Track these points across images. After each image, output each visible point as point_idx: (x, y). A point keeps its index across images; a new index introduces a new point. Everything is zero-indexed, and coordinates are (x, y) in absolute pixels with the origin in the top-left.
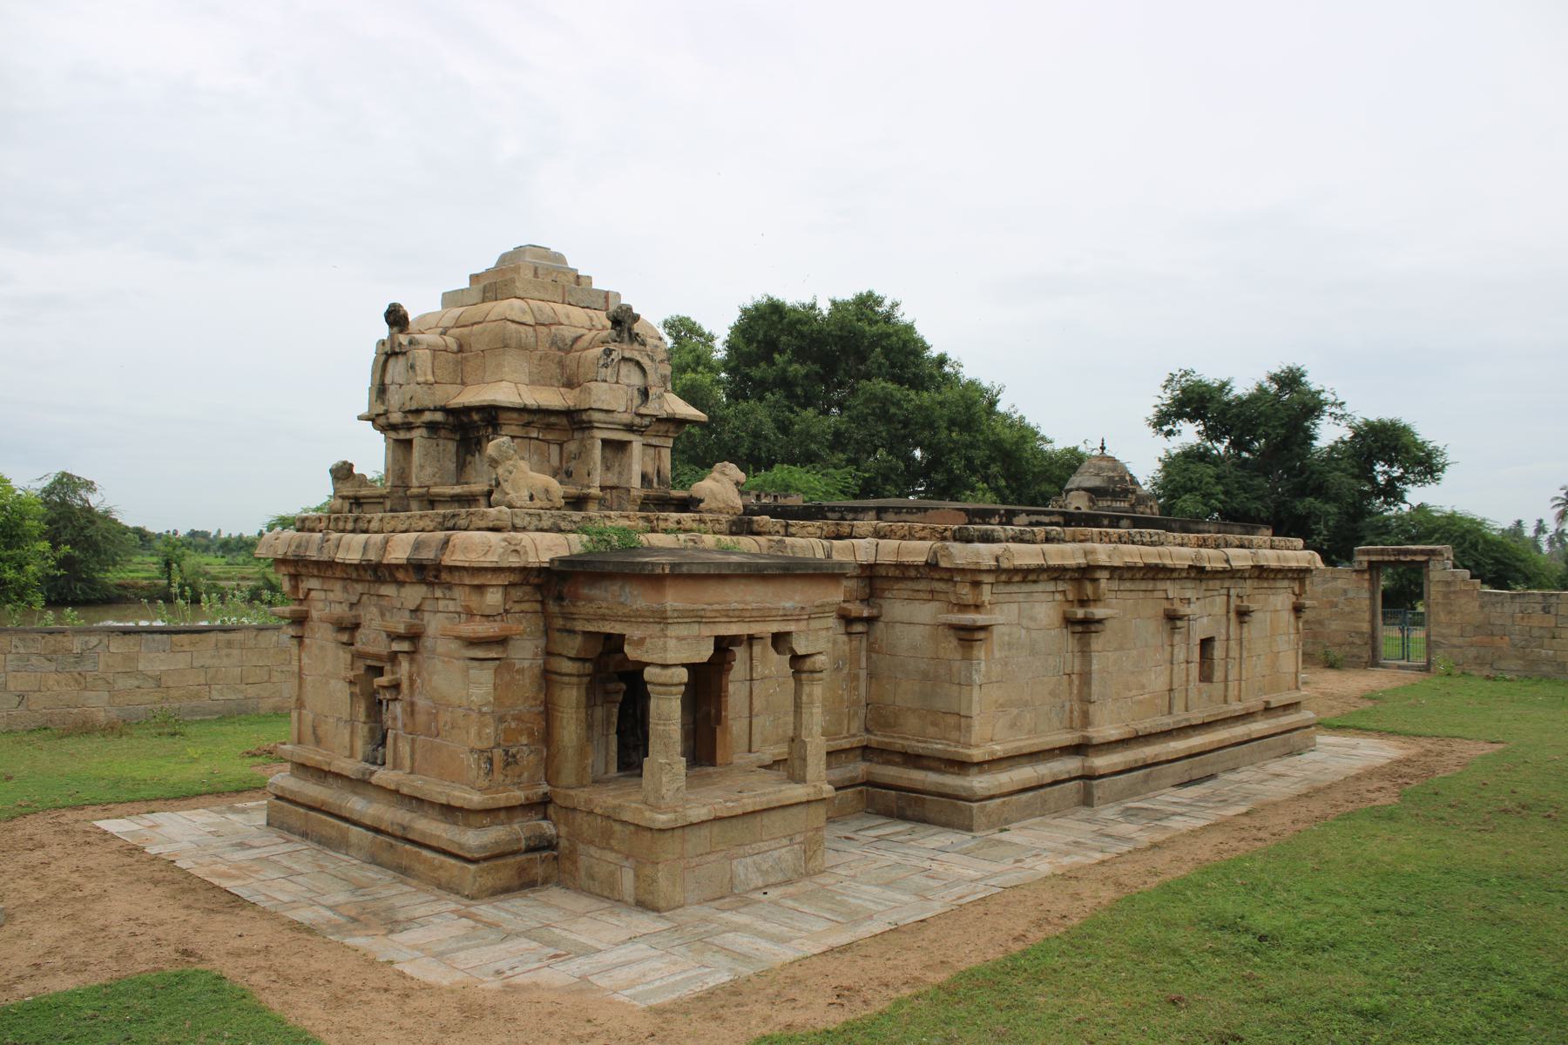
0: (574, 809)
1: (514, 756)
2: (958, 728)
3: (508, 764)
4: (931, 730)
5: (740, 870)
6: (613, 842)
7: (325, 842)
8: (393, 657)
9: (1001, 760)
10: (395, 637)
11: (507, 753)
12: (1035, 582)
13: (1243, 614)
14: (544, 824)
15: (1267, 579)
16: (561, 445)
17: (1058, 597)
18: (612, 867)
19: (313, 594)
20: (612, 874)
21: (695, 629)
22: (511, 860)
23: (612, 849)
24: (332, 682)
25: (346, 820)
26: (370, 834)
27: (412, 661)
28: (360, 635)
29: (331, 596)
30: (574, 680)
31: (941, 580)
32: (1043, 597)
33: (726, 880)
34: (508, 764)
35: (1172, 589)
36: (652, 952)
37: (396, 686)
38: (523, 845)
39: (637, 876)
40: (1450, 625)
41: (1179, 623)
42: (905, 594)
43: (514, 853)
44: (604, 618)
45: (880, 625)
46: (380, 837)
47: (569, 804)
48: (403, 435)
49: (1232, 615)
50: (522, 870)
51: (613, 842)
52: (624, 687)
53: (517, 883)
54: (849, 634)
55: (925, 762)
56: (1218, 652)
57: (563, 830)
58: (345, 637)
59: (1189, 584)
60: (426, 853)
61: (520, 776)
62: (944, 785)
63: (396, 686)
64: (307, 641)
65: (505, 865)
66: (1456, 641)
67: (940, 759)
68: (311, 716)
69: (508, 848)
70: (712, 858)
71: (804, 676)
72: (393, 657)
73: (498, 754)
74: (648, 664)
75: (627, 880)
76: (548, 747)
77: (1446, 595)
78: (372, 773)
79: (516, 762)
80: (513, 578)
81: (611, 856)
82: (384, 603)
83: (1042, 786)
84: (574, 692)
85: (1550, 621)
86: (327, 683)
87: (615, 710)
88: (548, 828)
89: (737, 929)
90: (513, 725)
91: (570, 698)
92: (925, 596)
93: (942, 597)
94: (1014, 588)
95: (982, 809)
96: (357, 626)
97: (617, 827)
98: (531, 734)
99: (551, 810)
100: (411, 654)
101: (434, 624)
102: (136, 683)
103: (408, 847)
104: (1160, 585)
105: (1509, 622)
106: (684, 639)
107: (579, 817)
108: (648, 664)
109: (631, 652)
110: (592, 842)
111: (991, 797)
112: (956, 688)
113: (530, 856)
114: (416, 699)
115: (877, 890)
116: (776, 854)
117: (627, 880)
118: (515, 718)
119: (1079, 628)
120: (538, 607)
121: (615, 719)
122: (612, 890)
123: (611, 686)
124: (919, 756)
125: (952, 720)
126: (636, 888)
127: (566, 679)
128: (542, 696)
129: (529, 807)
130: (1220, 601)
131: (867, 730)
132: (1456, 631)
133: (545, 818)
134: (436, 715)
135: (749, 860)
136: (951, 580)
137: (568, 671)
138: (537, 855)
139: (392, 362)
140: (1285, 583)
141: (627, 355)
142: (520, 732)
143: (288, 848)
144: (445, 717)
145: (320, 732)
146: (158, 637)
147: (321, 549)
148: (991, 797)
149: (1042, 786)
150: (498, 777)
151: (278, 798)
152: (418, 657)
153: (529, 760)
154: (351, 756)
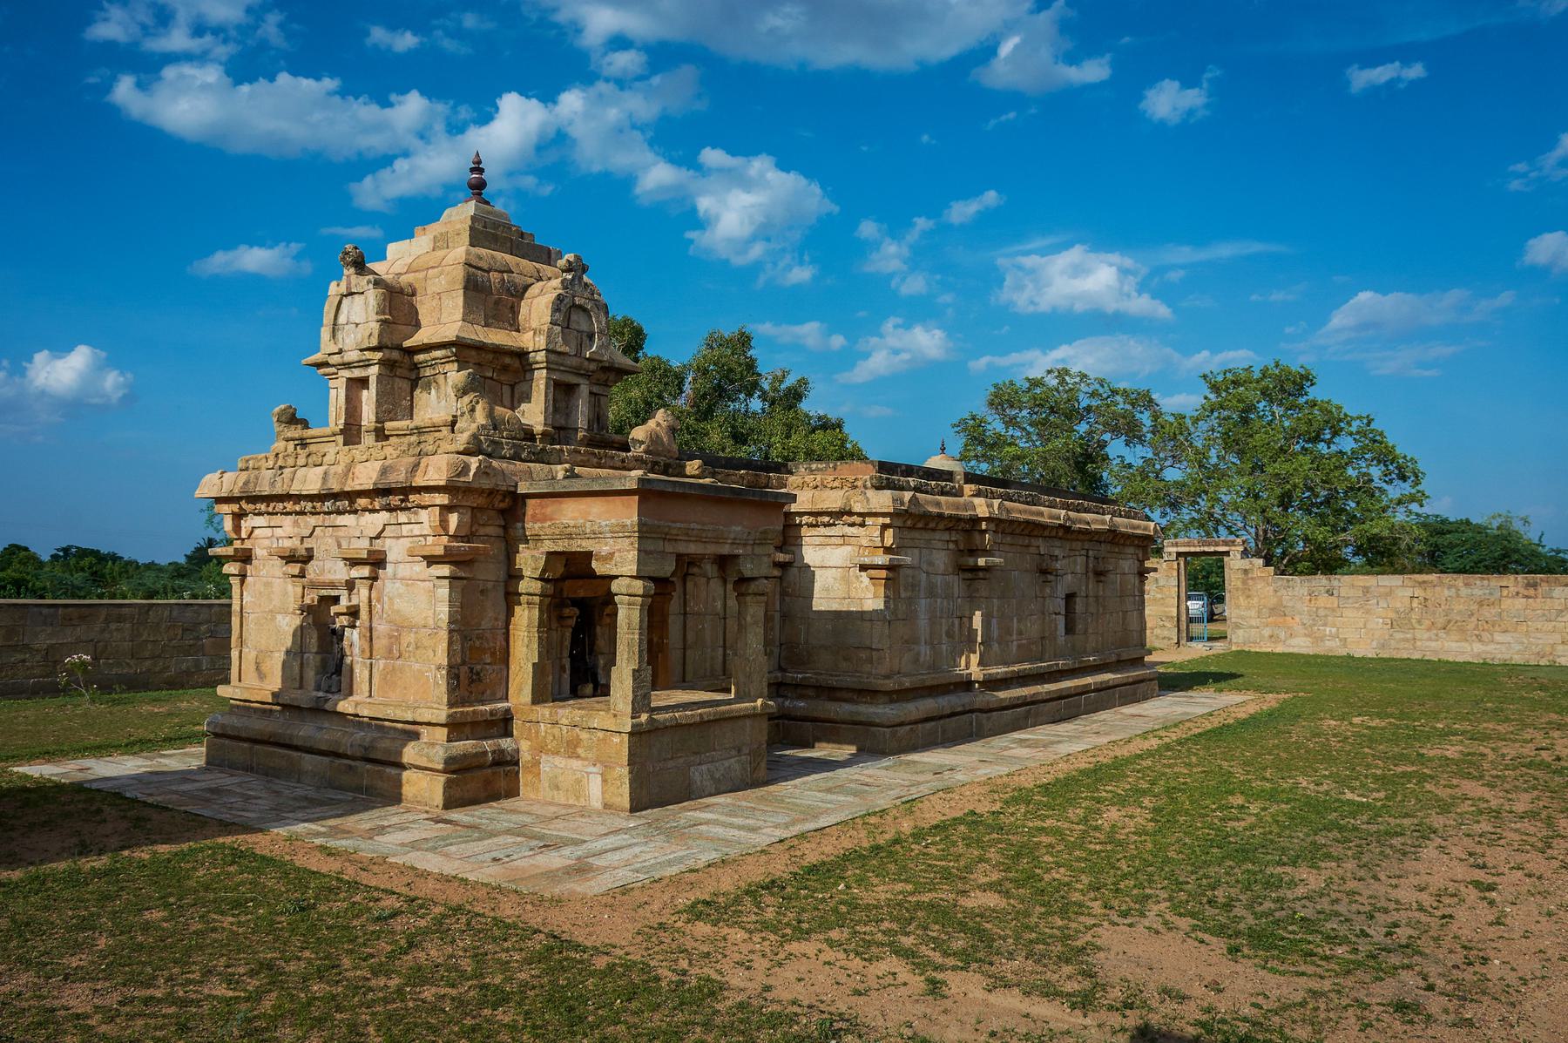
4: (844, 665)
5: (697, 777)
6: (580, 751)
7: (270, 773)
8: (350, 585)
9: (907, 690)
10: (354, 562)
12: (933, 530)
13: (1100, 574)
15: (1117, 544)
16: (512, 387)
17: (952, 546)
18: (579, 775)
19: (257, 532)
20: (578, 781)
21: (660, 545)
24: (279, 617)
25: (297, 748)
26: (326, 760)
28: (312, 568)
29: (278, 532)
32: (940, 545)
35: (1043, 546)
36: (1142, 304)
37: (354, 613)
39: (604, 781)
40: (1248, 608)
41: (1050, 578)
42: (818, 540)
45: (794, 571)
46: (338, 761)
48: (357, 373)
49: (1091, 575)
51: (580, 751)
52: (577, 611)
55: (838, 694)
56: (1079, 606)
58: (295, 569)
59: (1058, 543)
64: (249, 579)
66: (1254, 623)
67: (853, 690)
68: (253, 654)
71: (748, 598)
72: (350, 585)
74: (616, 577)
77: (1244, 582)
78: (327, 700)
80: (481, 501)
81: (576, 764)
82: (341, 533)
83: (941, 717)
86: (273, 619)
87: (568, 634)
89: (707, 822)
92: (840, 541)
94: (916, 534)
96: (308, 557)
97: (584, 735)
101: (395, 550)
103: (369, 766)
104: (1035, 542)
106: (651, 553)
109: (598, 567)
111: (902, 724)
112: (868, 624)
115: (820, 795)
116: (726, 764)
119: (969, 575)
120: (500, 531)
121: (567, 643)
123: (567, 611)
124: (833, 689)
125: (863, 655)
130: (1081, 560)
131: (781, 669)
132: (1253, 613)
134: (398, 638)
135: (704, 767)
136: (863, 525)
139: (345, 301)
140: (1131, 550)
143: (236, 780)
144: (408, 638)
145: (263, 668)
147: (273, 484)
148: (902, 724)
149: (941, 717)
151: (216, 735)
154: (301, 687)
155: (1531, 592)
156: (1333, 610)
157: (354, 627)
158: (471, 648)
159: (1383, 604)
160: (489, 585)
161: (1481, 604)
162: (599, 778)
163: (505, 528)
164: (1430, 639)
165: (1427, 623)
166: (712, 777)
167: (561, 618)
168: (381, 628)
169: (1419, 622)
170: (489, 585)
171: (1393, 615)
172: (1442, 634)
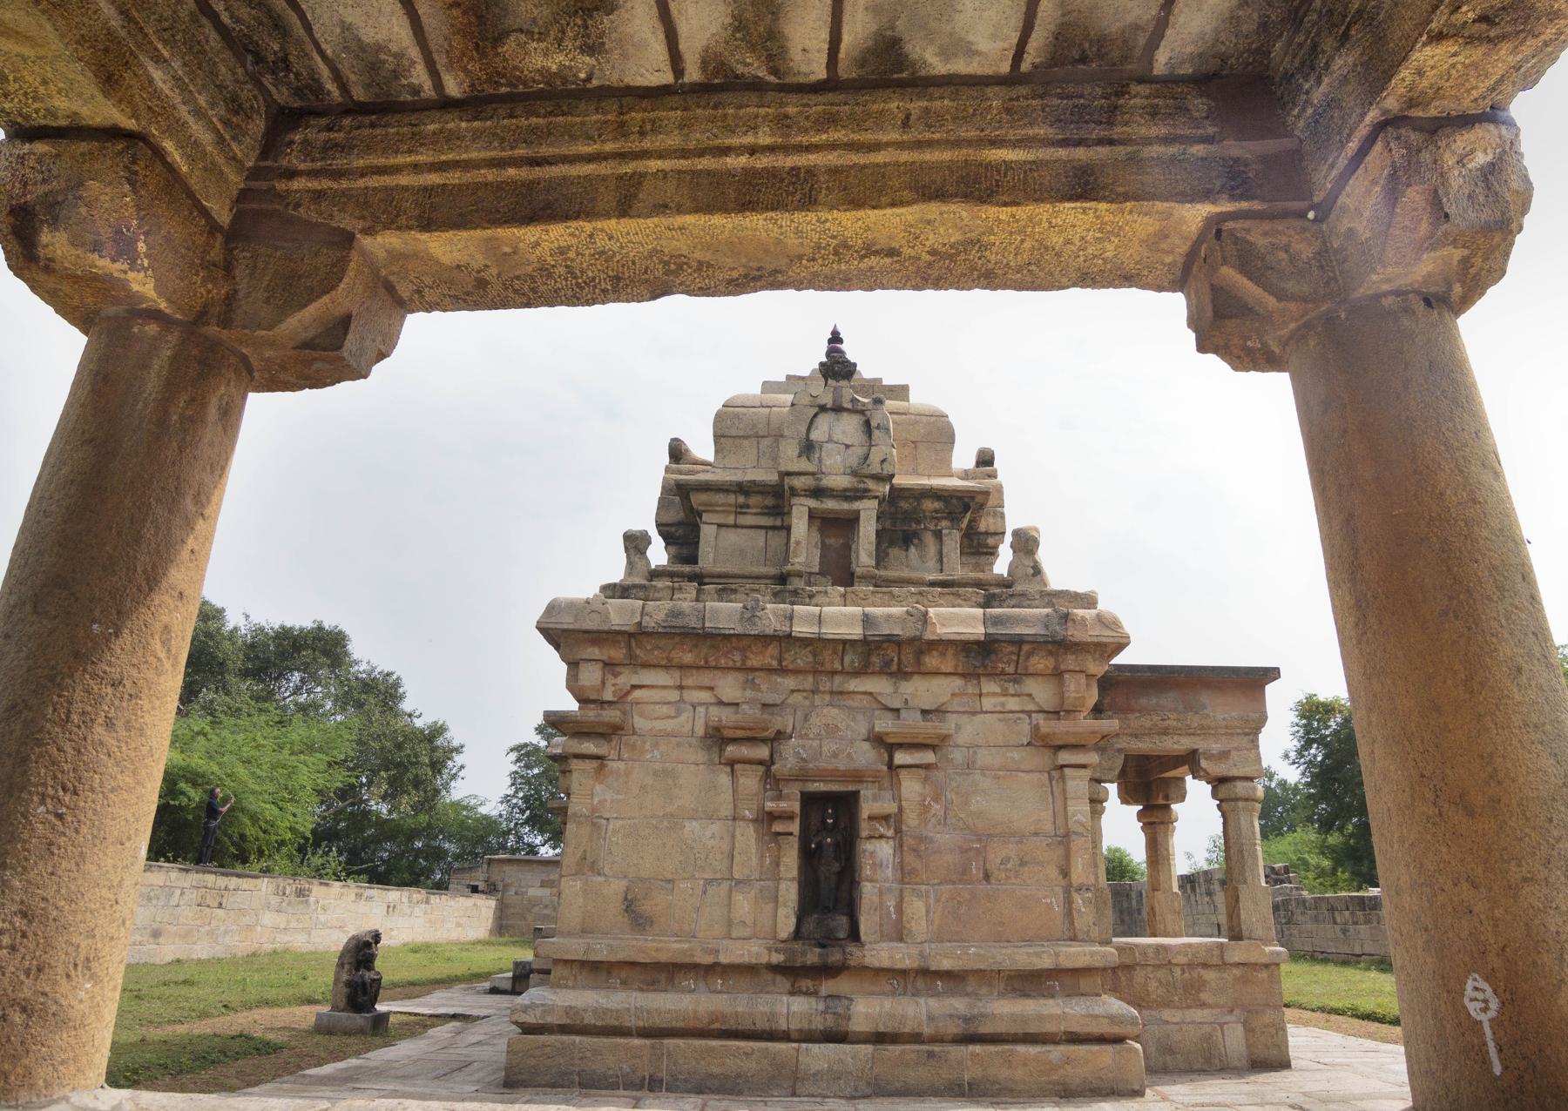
6: (1204, 996)
18: (1207, 1028)
20: (1208, 1038)
23: (1203, 1005)
44: (1165, 732)
51: (1204, 996)
107: (1139, 976)
110: (1167, 1004)
122: (1208, 1060)
126: (1249, 1046)
162: (1240, 1028)
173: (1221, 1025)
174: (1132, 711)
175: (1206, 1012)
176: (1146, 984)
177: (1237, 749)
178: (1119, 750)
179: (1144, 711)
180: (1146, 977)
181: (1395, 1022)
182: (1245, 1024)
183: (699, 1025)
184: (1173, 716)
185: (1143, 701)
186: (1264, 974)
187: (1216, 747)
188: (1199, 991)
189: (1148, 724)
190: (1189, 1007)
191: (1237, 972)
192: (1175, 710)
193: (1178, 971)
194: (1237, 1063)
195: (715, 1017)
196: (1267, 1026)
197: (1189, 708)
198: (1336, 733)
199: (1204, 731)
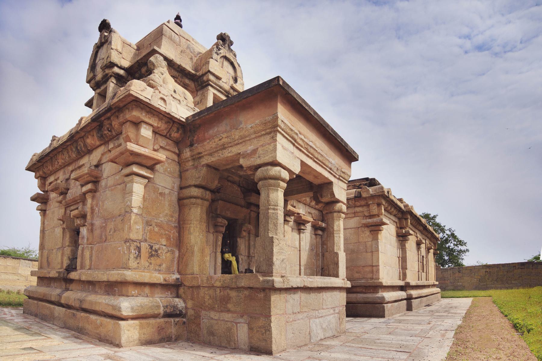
0: (198, 287)
1: (156, 251)
2: (372, 272)
3: (151, 256)
5: (314, 327)
6: (230, 306)
11: (151, 247)
14: (177, 300)
18: (229, 325)
20: (229, 330)
22: (152, 321)
23: (229, 311)
24: (56, 229)
27: (93, 198)
30: (199, 201)
31: (360, 206)
33: (308, 333)
34: (151, 256)
38: (161, 311)
39: (250, 329)
43: (155, 316)
44: (224, 147)
47: (195, 283)
50: (160, 329)
51: (230, 306)
53: (157, 337)
54: (316, 235)
57: (190, 304)
60: (93, 317)
61: (160, 266)
62: (368, 298)
63: (84, 216)
64: (47, 212)
65: (149, 324)
69: (150, 312)
70: (300, 316)
73: (144, 246)
75: (242, 333)
76: (179, 251)
79: (158, 256)
81: (227, 316)
84: (199, 210)
85: (461, 275)
86: (54, 231)
87: (220, 238)
88: (180, 303)
90: (156, 229)
91: (196, 214)
93: (360, 214)
95: (387, 306)
97: (233, 294)
98: (168, 239)
99: (181, 291)
100: (93, 191)
102: (18, 278)
105: (449, 276)
107: (202, 292)
108: (258, 167)
110: (212, 309)
113: (167, 319)
114: (94, 222)
117: (242, 333)
118: (157, 225)
121: (220, 243)
122: (229, 342)
126: (250, 338)
127: (193, 200)
128: (176, 215)
129: (165, 286)
133: (178, 296)
137: (195, 194)
138: (172, 320)
141: (228, 55)
142: (161, 235)
146: (27, 262)
150: (144, 262)
152: (98, 194)
153: (166, 255)
155: (523, 267)
156: (460, 277)
157: (84, 225)
158: (150, 231)
159: (476, 274)
160: (167, 191)
161: (507, 272)
162: (246, 327)
163: (179, 155)
164: (492, 284)
165: (491, 279)
166: (322, 328)
167: (215, 226)
168: (98, 222)
169: (488, 279)
170: (167, 191)
171: (480, 277)
172: (495, 282)
173: (237, 323)
174: (205, 140)
175: (230, 315)
176: (204, 297)
177: (262, 146)
178: (203, 166)
179: (212, 138)
180: (205, 293)
181: (37, 261)
182: (249, 324)
183: (40, 297)
184: (224, 135)
185: (211, 132)
186: (261, 295)
187: (250, 148)
188: (227, 303)
189: (214, 145)
190: (222, 311)
191: (246, 292)
192: (226, 131)
193: (218, 290)
194: (242, 346)
195: (45, 295)
196: (260, 327)
197: (235, 127)
198: (209, 80)
199: (243, 140)
